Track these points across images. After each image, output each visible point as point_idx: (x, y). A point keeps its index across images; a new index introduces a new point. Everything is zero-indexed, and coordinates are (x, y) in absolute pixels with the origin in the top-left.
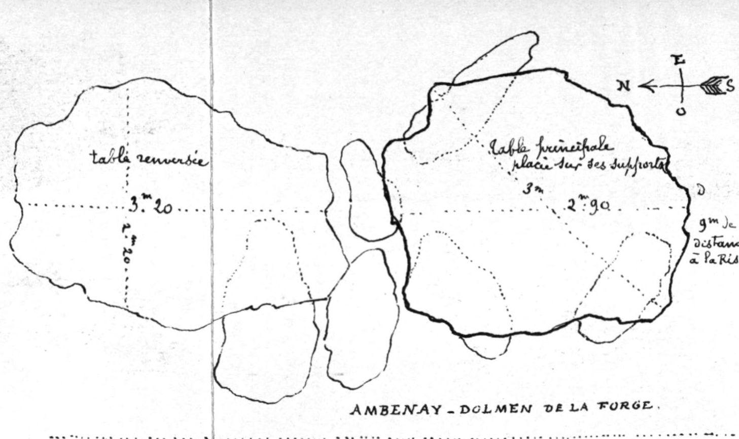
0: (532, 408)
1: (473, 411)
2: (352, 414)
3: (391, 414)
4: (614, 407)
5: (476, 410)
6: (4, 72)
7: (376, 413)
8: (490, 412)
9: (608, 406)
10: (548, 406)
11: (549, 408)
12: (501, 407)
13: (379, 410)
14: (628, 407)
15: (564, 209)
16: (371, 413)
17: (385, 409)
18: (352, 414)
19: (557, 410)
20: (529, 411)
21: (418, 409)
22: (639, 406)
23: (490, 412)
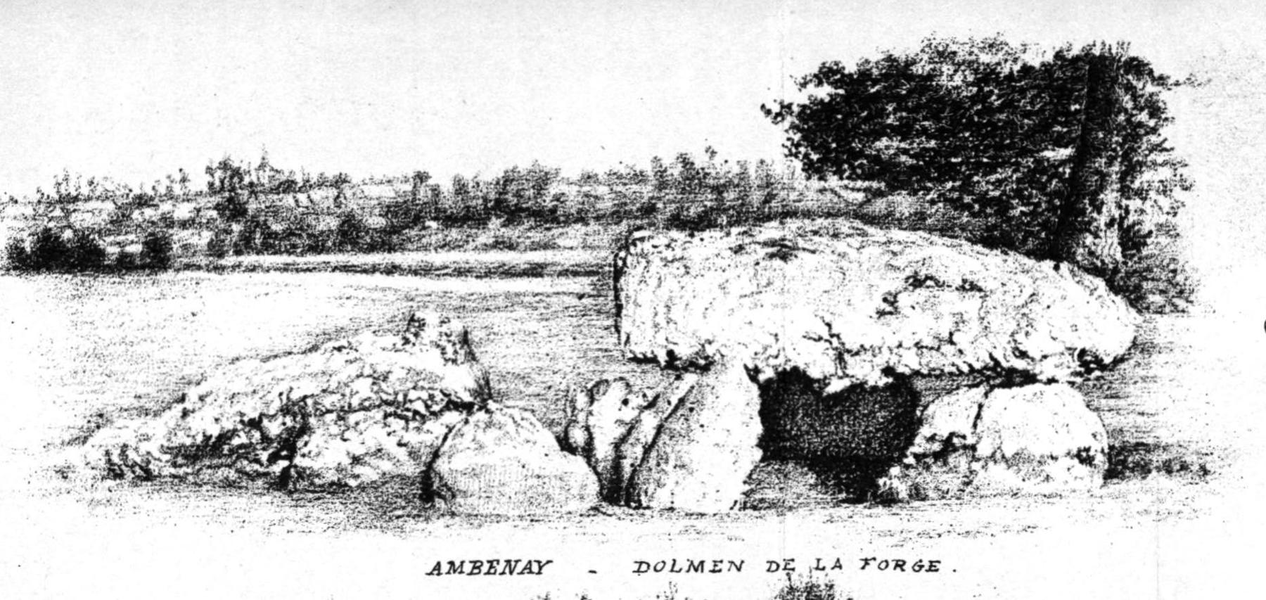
0: (744, 565)
1: (649, 565)
2: (431, 574)
3: (485, 574)
4: (659, 567)
5: (659, 567)
6: (1257, 95)
7: (702, 571)
8: (824, 569)
9: (873, 564)
10: (771, 562)
11: (774, 567)
12: (696, 564)
13: (468, 567)
14: (904, 567)
15: (1073, 438)
16: (696, 570)
17: (477, 565)
18: (549, 562)
19: (929, 570)
20: (739, 569)
21: (520, 567)
22: (921, 567)
23: (824, 569)
